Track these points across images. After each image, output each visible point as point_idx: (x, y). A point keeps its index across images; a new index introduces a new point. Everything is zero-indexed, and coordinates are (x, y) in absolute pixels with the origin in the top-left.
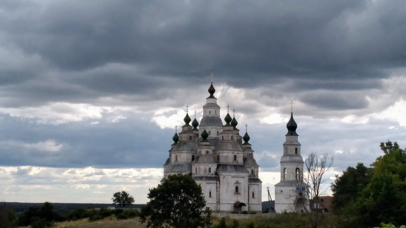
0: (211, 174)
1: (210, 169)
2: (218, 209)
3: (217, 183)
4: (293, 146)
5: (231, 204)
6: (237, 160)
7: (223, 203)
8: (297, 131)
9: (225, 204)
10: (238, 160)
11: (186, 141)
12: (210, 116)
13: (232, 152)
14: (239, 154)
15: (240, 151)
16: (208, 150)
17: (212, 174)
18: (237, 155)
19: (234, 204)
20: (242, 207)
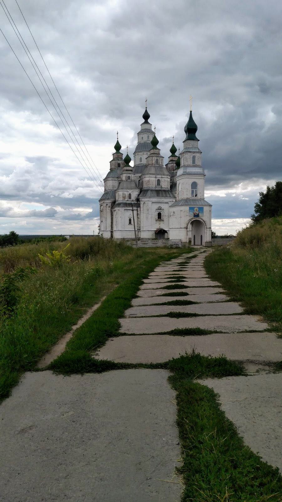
1: (130, 194)
3: (137, 210)
4: (189, 154)
7: (144, 230)
8: (198, 135)
12: (142, 142)
13: (155, 176)
14: (163, 179)
15: (164, 175)
18: (160, 179)
19: (155, 231)
20: (165, 233)
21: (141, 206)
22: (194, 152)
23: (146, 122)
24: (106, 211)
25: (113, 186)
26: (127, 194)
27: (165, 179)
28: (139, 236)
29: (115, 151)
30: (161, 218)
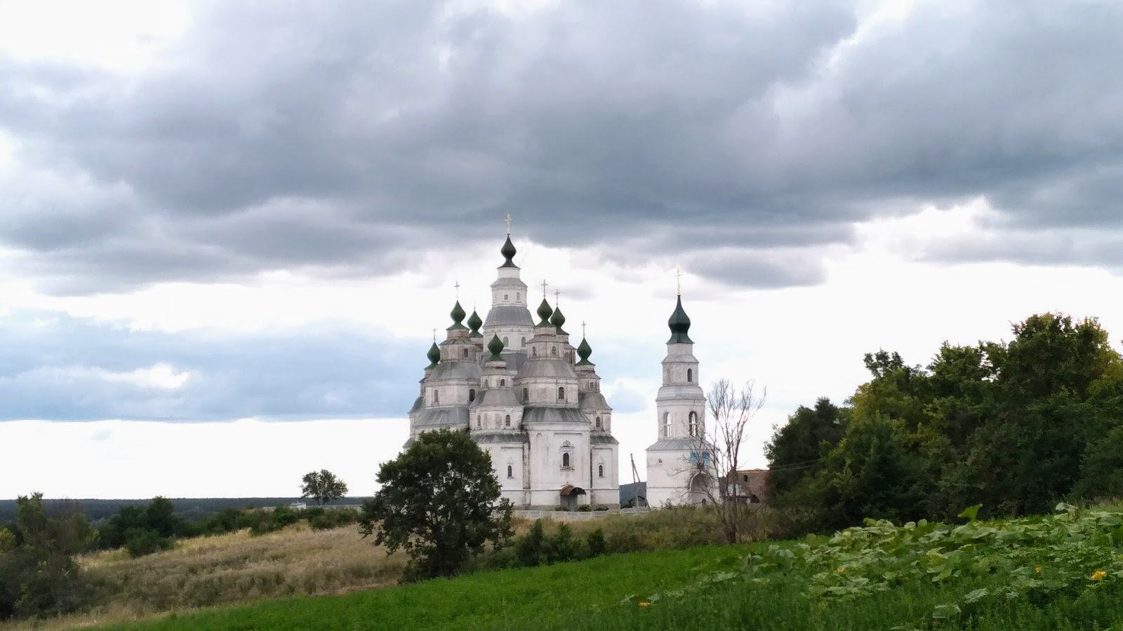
8: (691, 333)
12: (506, 304)
17: (514, 429)
21: (532, 439)
22: (690, 363)
23: (509, 264)
25: (459, 396)
28: (528, 502)
29: (452, 323)
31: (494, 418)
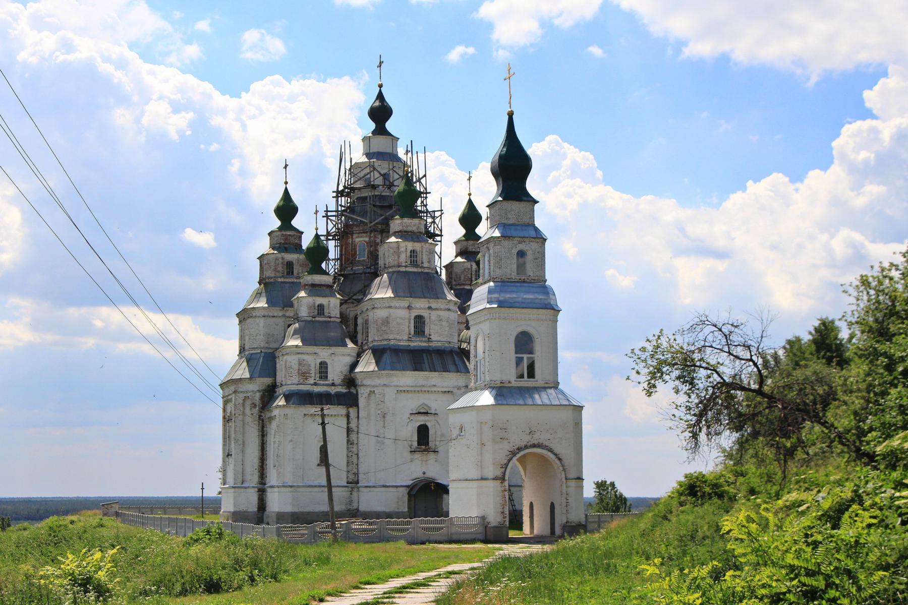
0: (327, 385)
1: (323, 367)
2: (355, 507)
3: (348, 416)
5: (397, 487)
6: (427, 332)
8: (533, 185)
9: (374, 487)
10: (431, 331)
11: (271, 278)
14: (434, 313)
16: (319, 300)
17: (333, 384)
18: (425, 313)
20: (442, 495)
21: (362, 401)
24: (243, 421)
26: (313, 362)
27: (442, 313)
28: (355, 506)
30: (427, 444)
31: (296, 367)
